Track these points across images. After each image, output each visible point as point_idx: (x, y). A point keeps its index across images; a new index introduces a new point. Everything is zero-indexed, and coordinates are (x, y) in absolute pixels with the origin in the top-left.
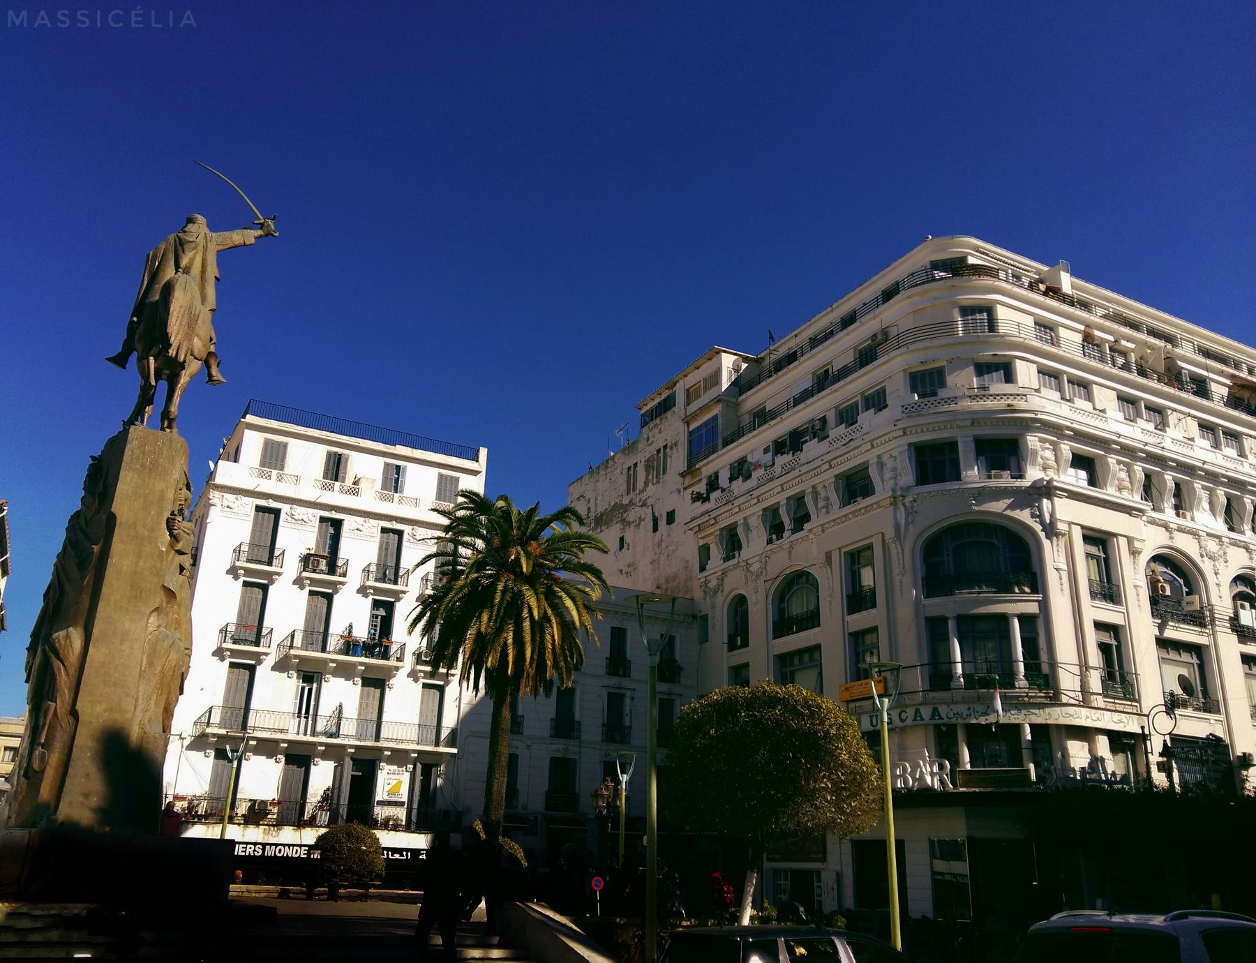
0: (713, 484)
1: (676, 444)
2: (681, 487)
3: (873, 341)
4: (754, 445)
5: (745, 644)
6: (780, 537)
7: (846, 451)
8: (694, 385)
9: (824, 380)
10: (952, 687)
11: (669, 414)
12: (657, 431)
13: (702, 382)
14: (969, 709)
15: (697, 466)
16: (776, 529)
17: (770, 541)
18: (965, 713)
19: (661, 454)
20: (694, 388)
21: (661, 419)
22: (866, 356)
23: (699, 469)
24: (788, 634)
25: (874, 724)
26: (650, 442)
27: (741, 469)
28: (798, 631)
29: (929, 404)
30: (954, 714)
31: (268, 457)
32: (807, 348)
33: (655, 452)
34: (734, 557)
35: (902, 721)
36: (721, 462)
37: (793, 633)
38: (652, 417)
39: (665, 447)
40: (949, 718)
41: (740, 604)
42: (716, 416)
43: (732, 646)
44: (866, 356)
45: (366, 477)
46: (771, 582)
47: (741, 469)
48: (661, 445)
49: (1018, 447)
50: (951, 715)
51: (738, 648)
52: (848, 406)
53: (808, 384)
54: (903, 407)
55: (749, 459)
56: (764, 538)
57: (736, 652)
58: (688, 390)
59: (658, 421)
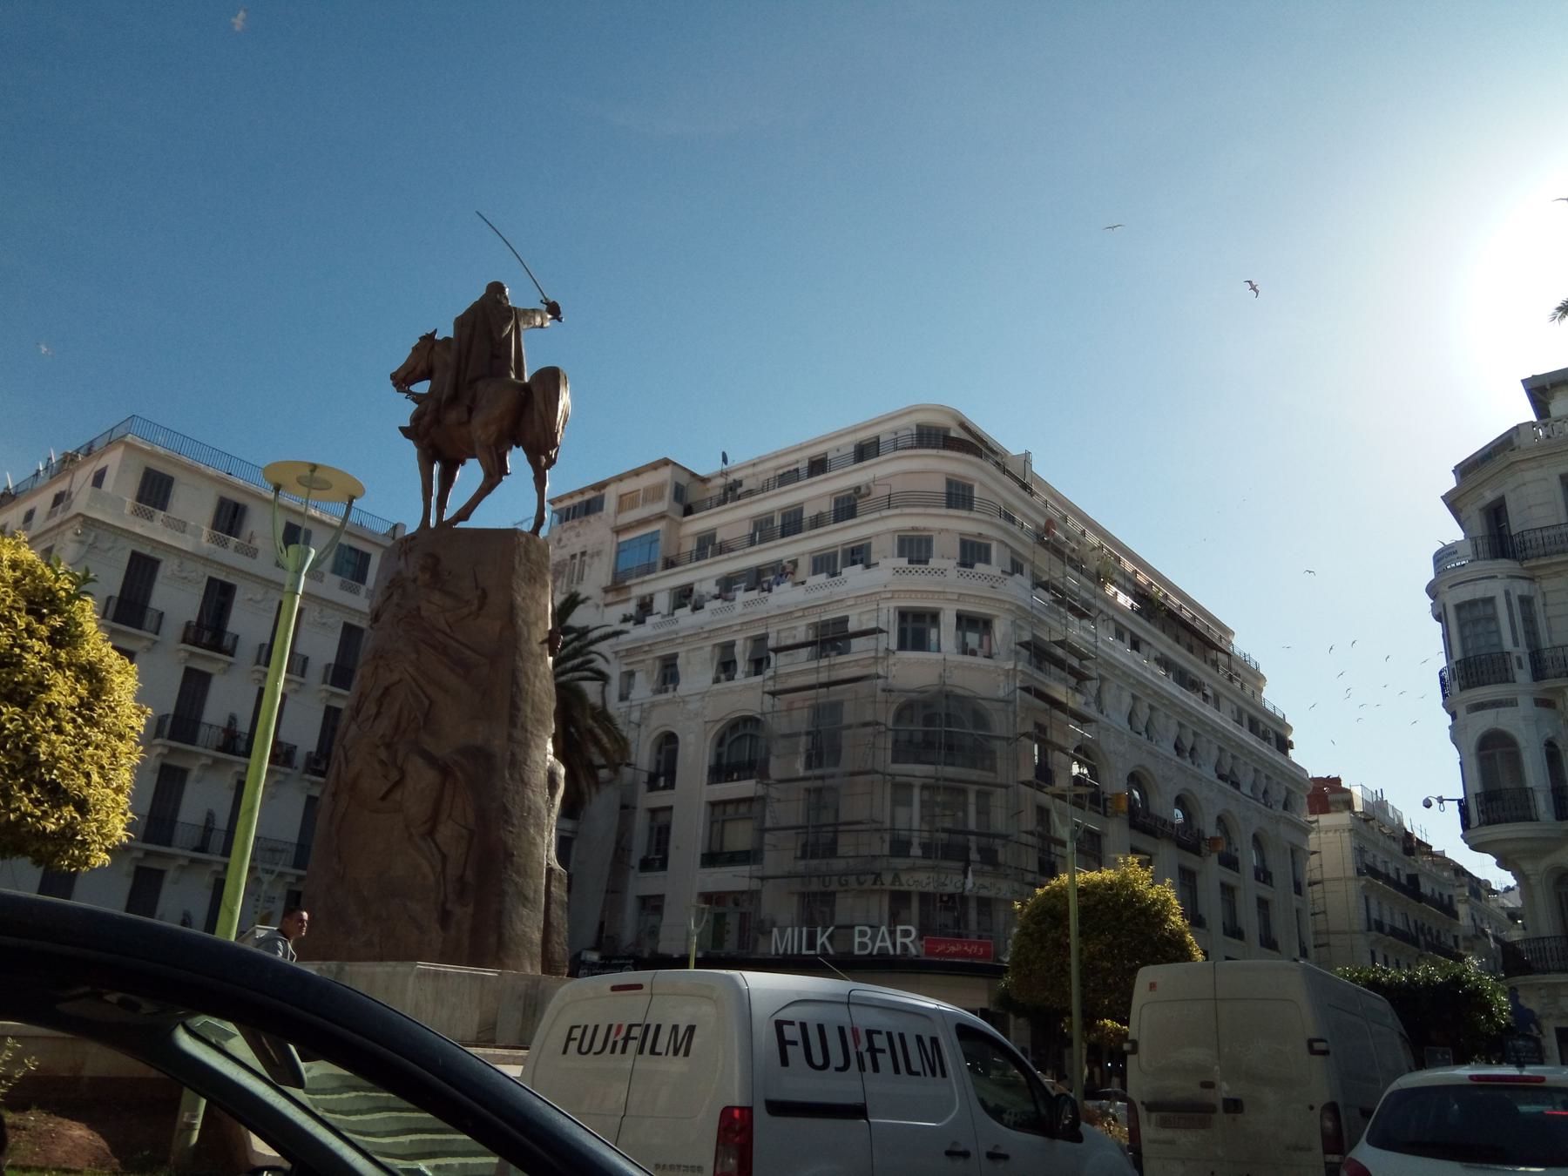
0: (645, 607)
1: (598, 553)
2: (601, 604)
3: (855, 492)
4: (704, 576)
5: (670, 784)
6: (730, 678)
7: (989, 595)
8: (631, 493)
9: (792, 523)
10: (911, 854)
11: (592, 518)
12: (572, 534)
13: (642, 492)
14: (929, 878)
15: (628, 583)
16: (727, 667)
17: (717, 680)
18: (925, 881)
19: (577, 561)
20: (631, 495)
21: (581, 522)
22: (846, 507)
23: (629, 587)
24: (726, 781)
25: (827, 884)
26: (561, 545)
27: (684, 596)
28: (739, 779)
29: (913, 571)
30: (915, 882)
31: (947, 783)
32: (803, 472)
33: (568, 557)
34: (666, 691)
35: (860, 884)
36: (661, 586)
37: (732, 781)
38: (574, 512)
39: (583, 554)
40: (909, 885)
41: (669, 741)
42: (659, 531)
43: (652, 784)
44: (846, 507)
45: (1329, 918)
46: (711, 724)
47: (684, 596)
48: (577, 550)
49: (991, 627)
50: (911, 883)
51: (659, 789)
52: (825, 554)
53: (988, 466)
54: (894, 569)
55: (696, 587)
56: (711, 674)
57: (656, 793)
58: (621, 496)
59: (576, 523)
